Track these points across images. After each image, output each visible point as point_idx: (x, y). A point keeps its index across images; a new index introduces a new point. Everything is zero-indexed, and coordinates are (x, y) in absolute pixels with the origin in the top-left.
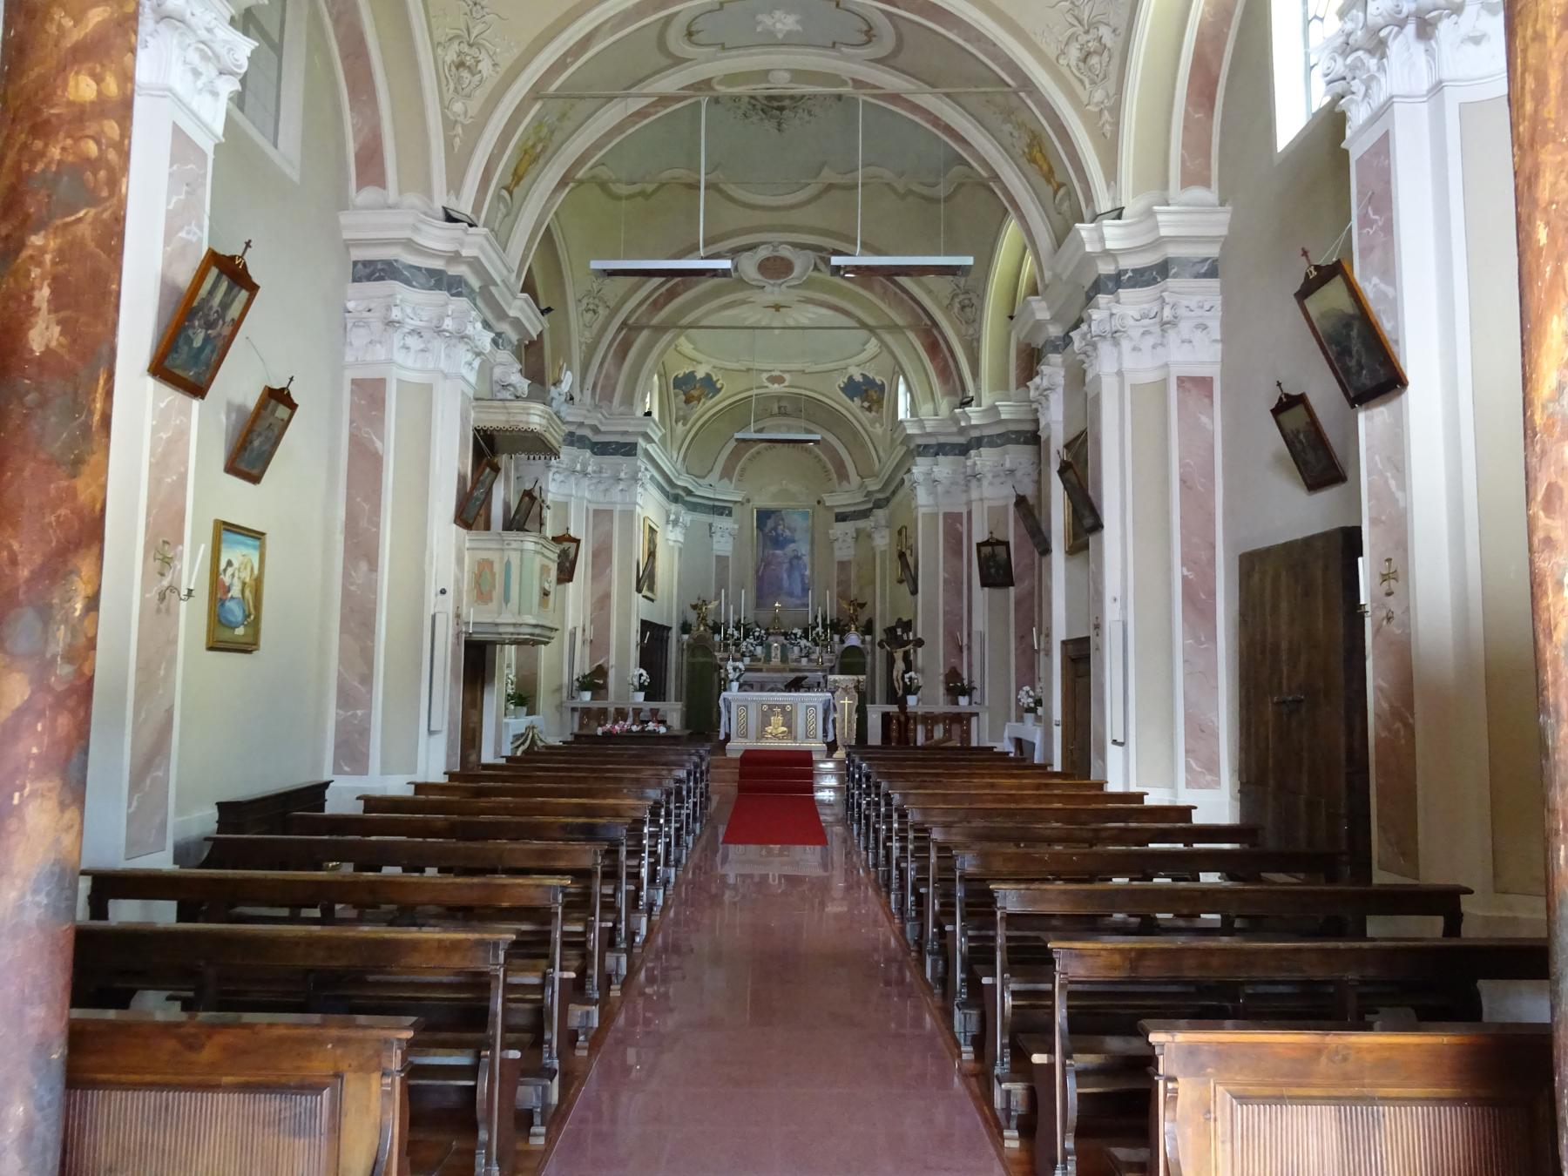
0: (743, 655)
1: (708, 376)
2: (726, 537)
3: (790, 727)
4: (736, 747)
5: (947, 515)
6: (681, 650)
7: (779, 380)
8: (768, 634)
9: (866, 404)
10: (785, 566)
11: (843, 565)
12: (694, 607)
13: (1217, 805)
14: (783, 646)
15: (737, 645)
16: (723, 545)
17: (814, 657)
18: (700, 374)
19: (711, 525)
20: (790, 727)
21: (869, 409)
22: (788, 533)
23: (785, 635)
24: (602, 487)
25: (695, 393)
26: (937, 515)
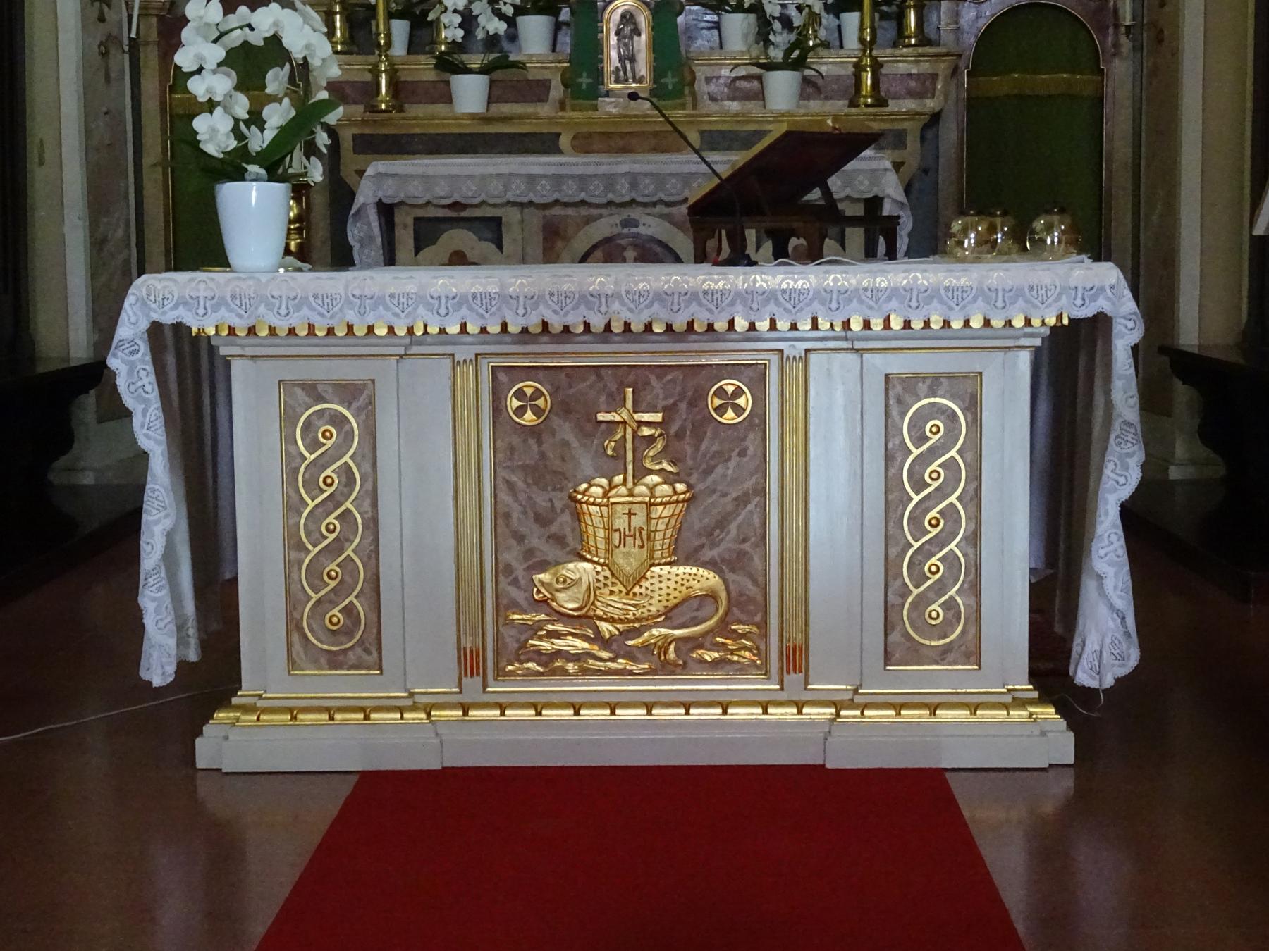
0: (450, 64)
17: (829, 65)
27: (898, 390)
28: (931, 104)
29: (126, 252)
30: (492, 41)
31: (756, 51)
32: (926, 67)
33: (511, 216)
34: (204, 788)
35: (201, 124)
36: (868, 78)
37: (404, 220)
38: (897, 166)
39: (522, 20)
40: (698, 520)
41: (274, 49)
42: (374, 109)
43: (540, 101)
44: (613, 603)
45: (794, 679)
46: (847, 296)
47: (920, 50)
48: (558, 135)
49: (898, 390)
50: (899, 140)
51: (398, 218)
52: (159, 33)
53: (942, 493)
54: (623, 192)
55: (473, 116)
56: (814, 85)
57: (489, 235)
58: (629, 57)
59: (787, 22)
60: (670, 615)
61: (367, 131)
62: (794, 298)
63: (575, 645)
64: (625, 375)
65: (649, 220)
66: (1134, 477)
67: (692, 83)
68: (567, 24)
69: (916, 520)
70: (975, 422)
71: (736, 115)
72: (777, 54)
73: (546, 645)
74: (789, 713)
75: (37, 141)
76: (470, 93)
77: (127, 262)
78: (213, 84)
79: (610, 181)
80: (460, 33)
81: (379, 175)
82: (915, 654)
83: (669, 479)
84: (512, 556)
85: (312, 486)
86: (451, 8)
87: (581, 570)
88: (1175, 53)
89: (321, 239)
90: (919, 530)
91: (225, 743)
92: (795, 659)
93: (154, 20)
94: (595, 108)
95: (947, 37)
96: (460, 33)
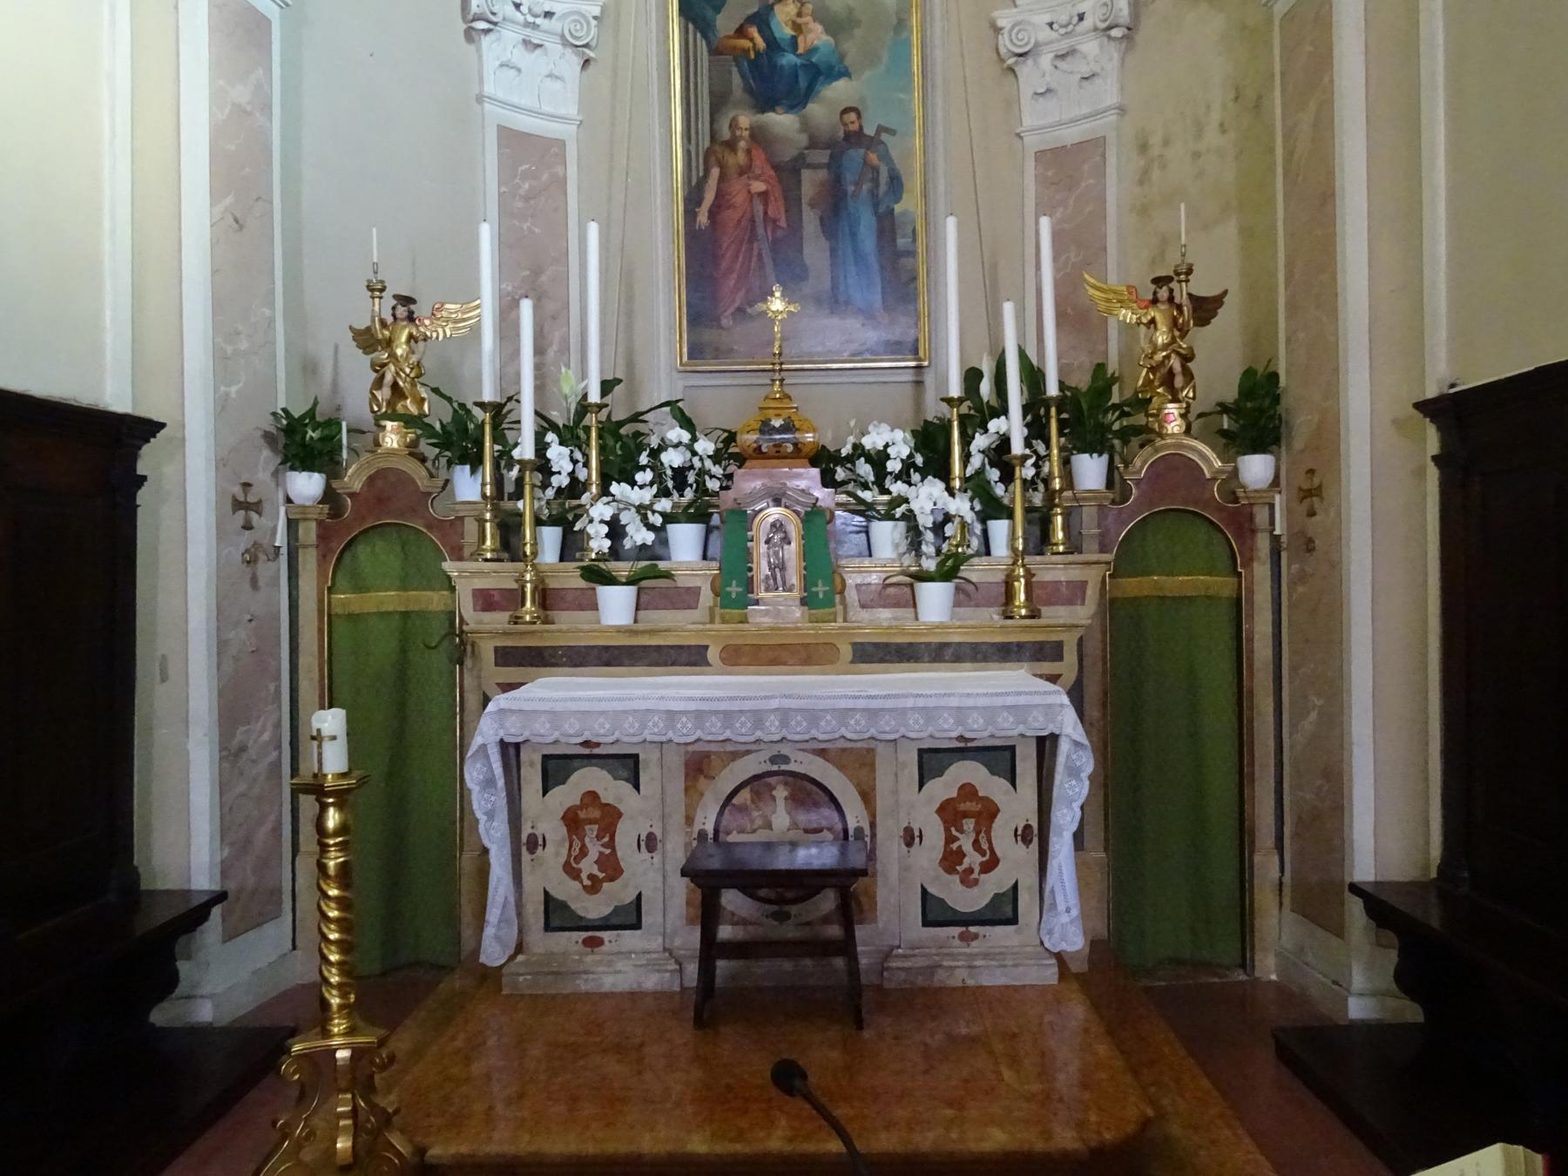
0: (597, 576)
11: (1067, 168)
12: (366, 340)
13: (1421, 1019)
14: (814, 517)
15: (566, 519)
17: (975, 571)
22: (816, 36)
23: (825, 461)
29: (275, 754)
30: (643, 551)
31: (908, 560)
32: (1075, 574)
33: (648, 757)
36: (1020, 586)
39: (673, 529)
42: (516, 620)
43: (690, 608)
47: (1070, 558)
48: (707, 647)
51: (525, 755)
52: (318, 536)
55: (619, 630)
56: (967, 595)
57: (625, 774)
61: (509, 643)
65: (801, 756)
67: (842, 592)
68: (717, 528)
71: (890, 628)
72: (930, 565)
75: (159, 654)
77: (277, 764)
80: (608, 543)
81: (502, 711)
86: (597, 519)
93: (313, 525)
94: (744, 620)
96: (608, 543)
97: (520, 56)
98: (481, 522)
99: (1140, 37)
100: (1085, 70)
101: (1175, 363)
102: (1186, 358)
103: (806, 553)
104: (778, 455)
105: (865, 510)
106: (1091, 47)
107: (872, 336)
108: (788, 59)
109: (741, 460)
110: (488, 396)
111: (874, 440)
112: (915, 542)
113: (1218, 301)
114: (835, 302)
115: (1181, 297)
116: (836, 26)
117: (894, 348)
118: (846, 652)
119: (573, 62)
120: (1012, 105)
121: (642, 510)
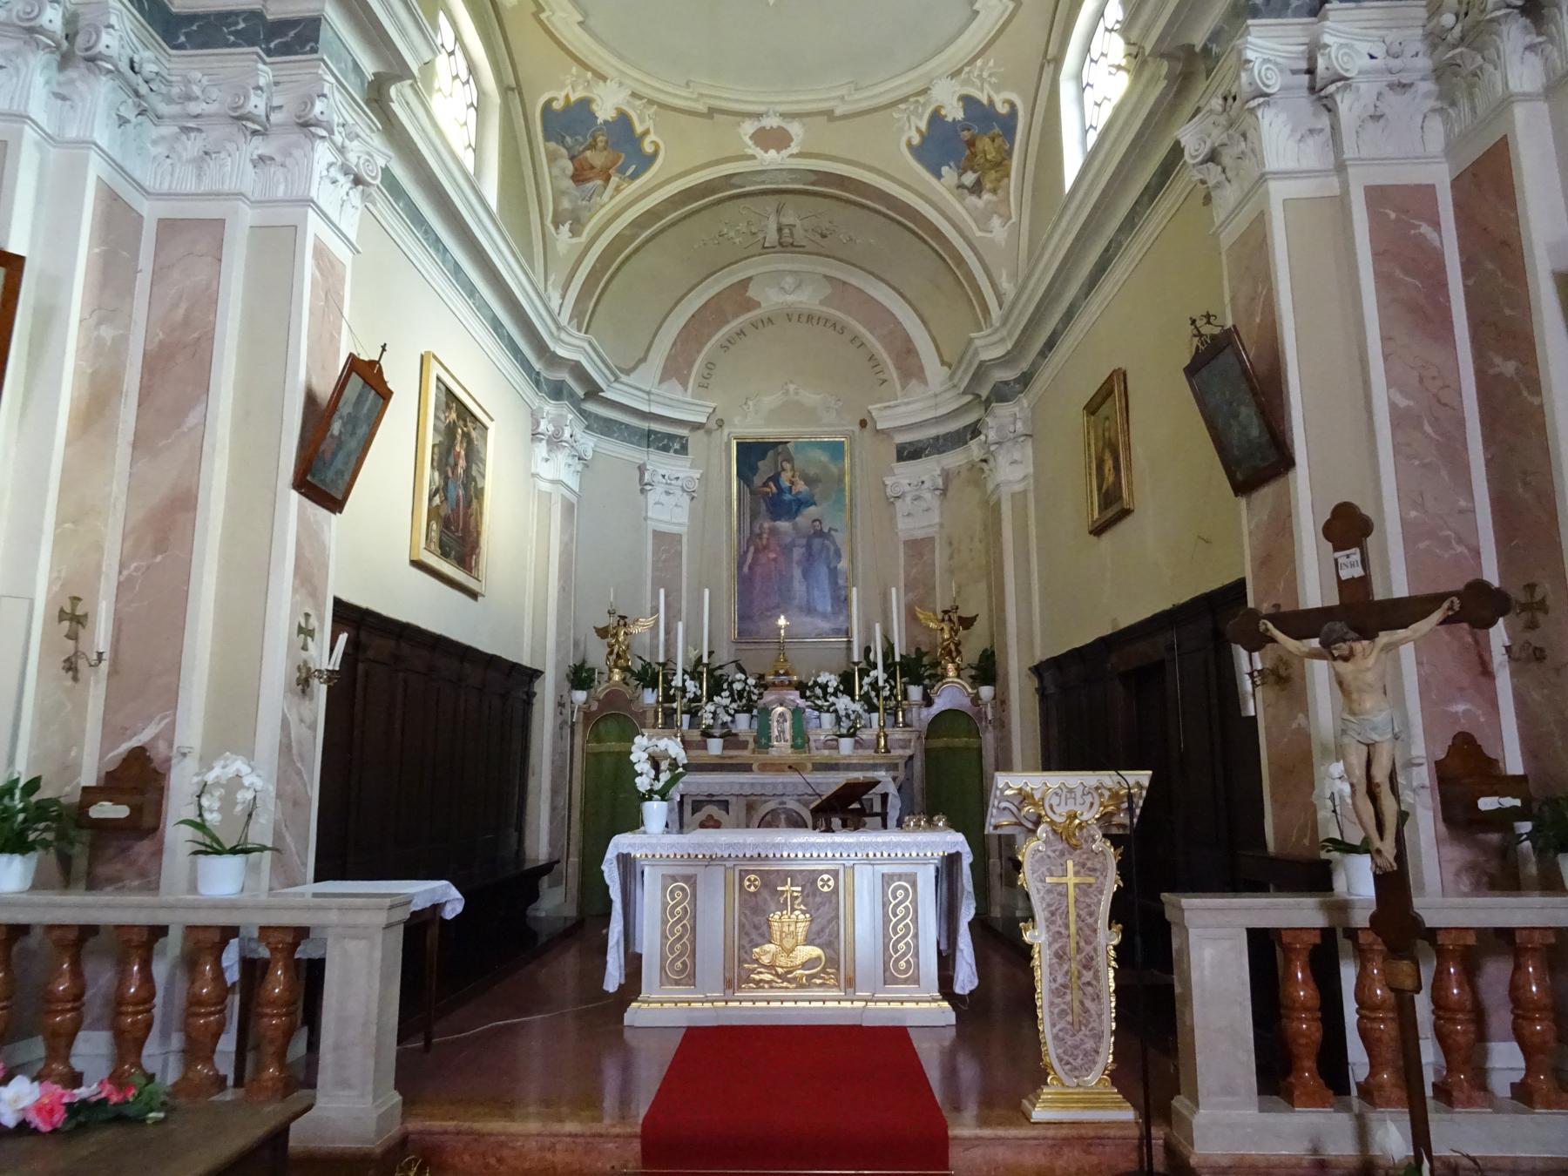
0: (707, 734)
1: (623, 120)
2: (682, 498)
3: (830, 945)
4: (661, 1009)
5: (1377, 196)
6: (565, 727)
7: (778, 139)
8: (763, 685)
9: (969, 178)
10: (797, 553)
11: (918, 548)
12: (603, 633)
14: (797, 712)
15: (694, 713)
16: (669, 511)
17: (865, 735)
18: (604, 112)
19: (642, 469)
20: (830, 945)
21: (977, 189)
22: (801, 486)
23: (802, 687)
24: (192, 146)
25: (596, 158)
26: (1342, 203)
27: (887, 879)
28: (909, 752)
30: (724, 724)
32: (906, 736)
33: (732, 800)
34: (627, 1035)
35: (638, 780)
37: (688, 801)
38: (894, 779)
40: (815, 928)
41: (666, 755)
44: (782, 960)
45: (850, 990)
46: (867, 845)
49: (887, 879)
50: (895, 767)
53: (904, 918)
54: (779, 791)
58: (782, 732)
59: (848, 716)
60: (804, 966)
62: (848, 846)
63: (768, 977)
64: (788, 873)
66: (973, 912)
69: (895, 928)
70: (915, 891)
72: (844, 731)
73: (757, 977)
74: (848, 1004)
76: (715, 746)
78: (643, 766)
79: (774, 785)
82: (896, 981)
83: (804, 912)
84: (745, 942)
85: (673, 916)
87: (767, 947)
88: (1010, 732)
89: (679, 823)
90: (896, 933)
91: (636, 1014)
92: (851, 983)
95: (915, 723)
97: (664, 499)
98: (656, 712)
99: (949, 494)
100: (925, 506)
101: (952, 647)
102: (957, 645)
103: (793, 726)
104: (782, 685)
105: (819, 709)
106: (927, 495)
107: (826, 625)
108: (787, 497)
109: (766, 687)
110: (661, 660)
111: (822, 679)
112: (838, 720)
113: (974, 619)
114: (810, 610)
115: (955, 619)
116: (809, 481)
117: (836, 632)
118: (810, 766)
119: (687, 498)
120: (892, 518)
121: (726, 707)
